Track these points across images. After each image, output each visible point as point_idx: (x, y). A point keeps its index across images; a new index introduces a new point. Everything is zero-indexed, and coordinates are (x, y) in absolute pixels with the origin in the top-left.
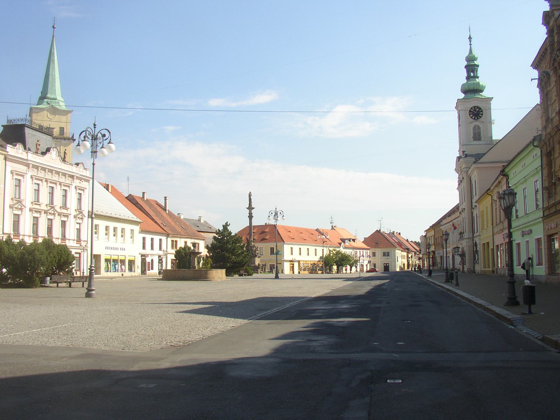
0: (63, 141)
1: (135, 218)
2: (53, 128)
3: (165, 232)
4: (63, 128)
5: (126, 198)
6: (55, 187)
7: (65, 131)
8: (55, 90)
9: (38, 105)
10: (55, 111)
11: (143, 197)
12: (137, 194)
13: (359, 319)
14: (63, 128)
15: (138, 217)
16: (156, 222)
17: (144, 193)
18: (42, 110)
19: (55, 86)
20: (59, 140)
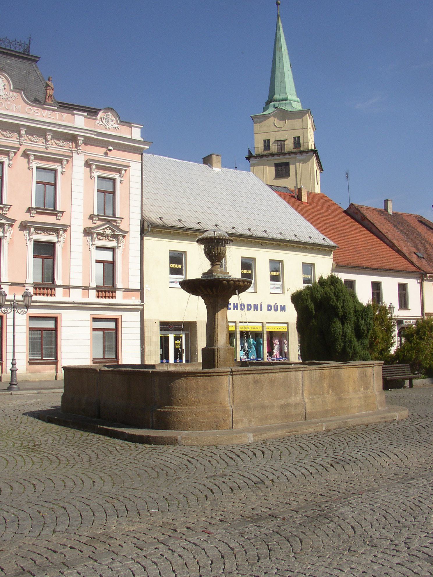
0: (299, 157)
1: (318, 237)
2: (284, 141)
3: (415, 269)
4: (299, 138)
5: (346, 212)
6: (118, 179)
7: (301, 141)
8: (285, 88)
9: (263, 112)
10: (285, 115)
11: (386, 209)
12: (368, 202)
13: (112, 428)
14: (299, 138)
15: (321, 229)
16: (398, 251)
17: (386, 201)
18: (267, 117)
19: (284, 83)
20: (293, 156)
